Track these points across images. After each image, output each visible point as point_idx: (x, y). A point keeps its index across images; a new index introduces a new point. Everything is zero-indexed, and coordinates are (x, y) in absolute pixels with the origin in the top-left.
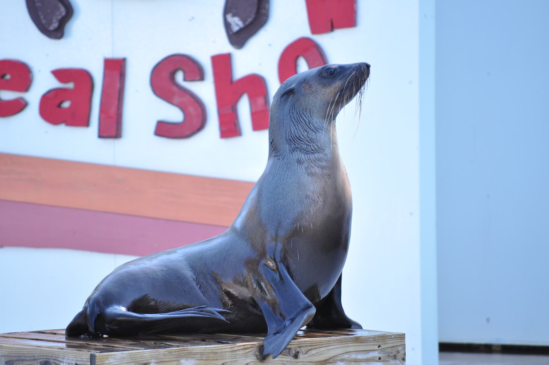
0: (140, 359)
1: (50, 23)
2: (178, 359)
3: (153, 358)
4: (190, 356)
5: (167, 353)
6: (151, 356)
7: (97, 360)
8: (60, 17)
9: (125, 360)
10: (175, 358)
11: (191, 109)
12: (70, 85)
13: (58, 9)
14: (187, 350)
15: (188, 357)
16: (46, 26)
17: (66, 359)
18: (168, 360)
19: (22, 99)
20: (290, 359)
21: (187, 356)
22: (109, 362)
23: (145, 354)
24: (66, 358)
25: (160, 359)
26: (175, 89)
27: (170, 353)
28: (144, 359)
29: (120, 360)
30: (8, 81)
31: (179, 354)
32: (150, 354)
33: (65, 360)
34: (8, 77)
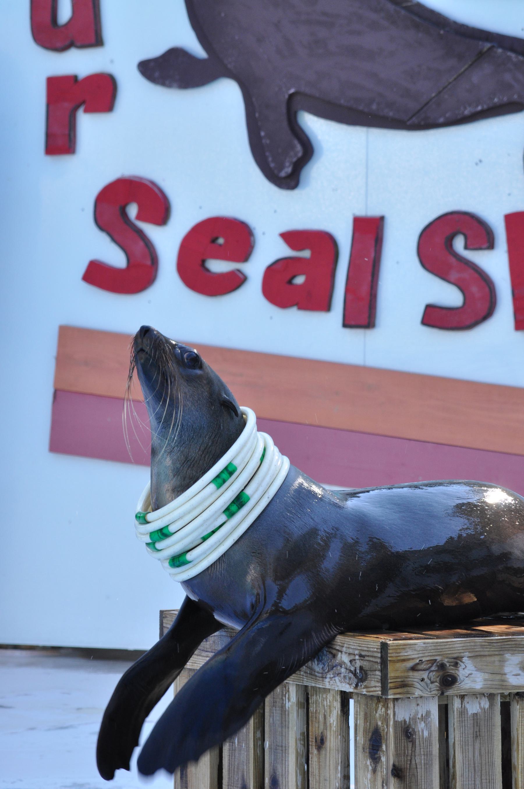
0: (449, 651)
1: (281, 167)
2: (501, 652)
3: (466, 651)
4: (517, 649)
5: (486, 644)
6: (464, 648)
7: (389, 651)
8: (295, 160)
9: (428, 651)
10: (497, 651)
11: (474, 289)
12: (306, 254)
13: (293, 147)
14: (515, 641)
15: (515, 650)
16: (276, 172)
17: (346, 647)
18: (487, 653)
19: (239, 271)
20: (139, 507)
21: (514, 649)
22: (406, 654)
23: (455, 644)
24: (345, 645)
25: (477, 651)
26: (452, 260)
27: (490, 643)
28: (455, 652)
29: (421, 652)
30: (220, 246)
31: (503, 647)
32: (462, 645)
33: (344, 649)
34: (221, 241)
